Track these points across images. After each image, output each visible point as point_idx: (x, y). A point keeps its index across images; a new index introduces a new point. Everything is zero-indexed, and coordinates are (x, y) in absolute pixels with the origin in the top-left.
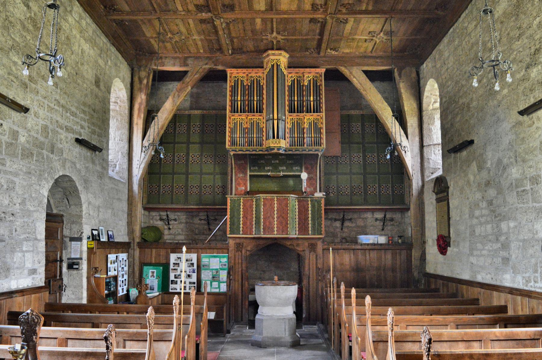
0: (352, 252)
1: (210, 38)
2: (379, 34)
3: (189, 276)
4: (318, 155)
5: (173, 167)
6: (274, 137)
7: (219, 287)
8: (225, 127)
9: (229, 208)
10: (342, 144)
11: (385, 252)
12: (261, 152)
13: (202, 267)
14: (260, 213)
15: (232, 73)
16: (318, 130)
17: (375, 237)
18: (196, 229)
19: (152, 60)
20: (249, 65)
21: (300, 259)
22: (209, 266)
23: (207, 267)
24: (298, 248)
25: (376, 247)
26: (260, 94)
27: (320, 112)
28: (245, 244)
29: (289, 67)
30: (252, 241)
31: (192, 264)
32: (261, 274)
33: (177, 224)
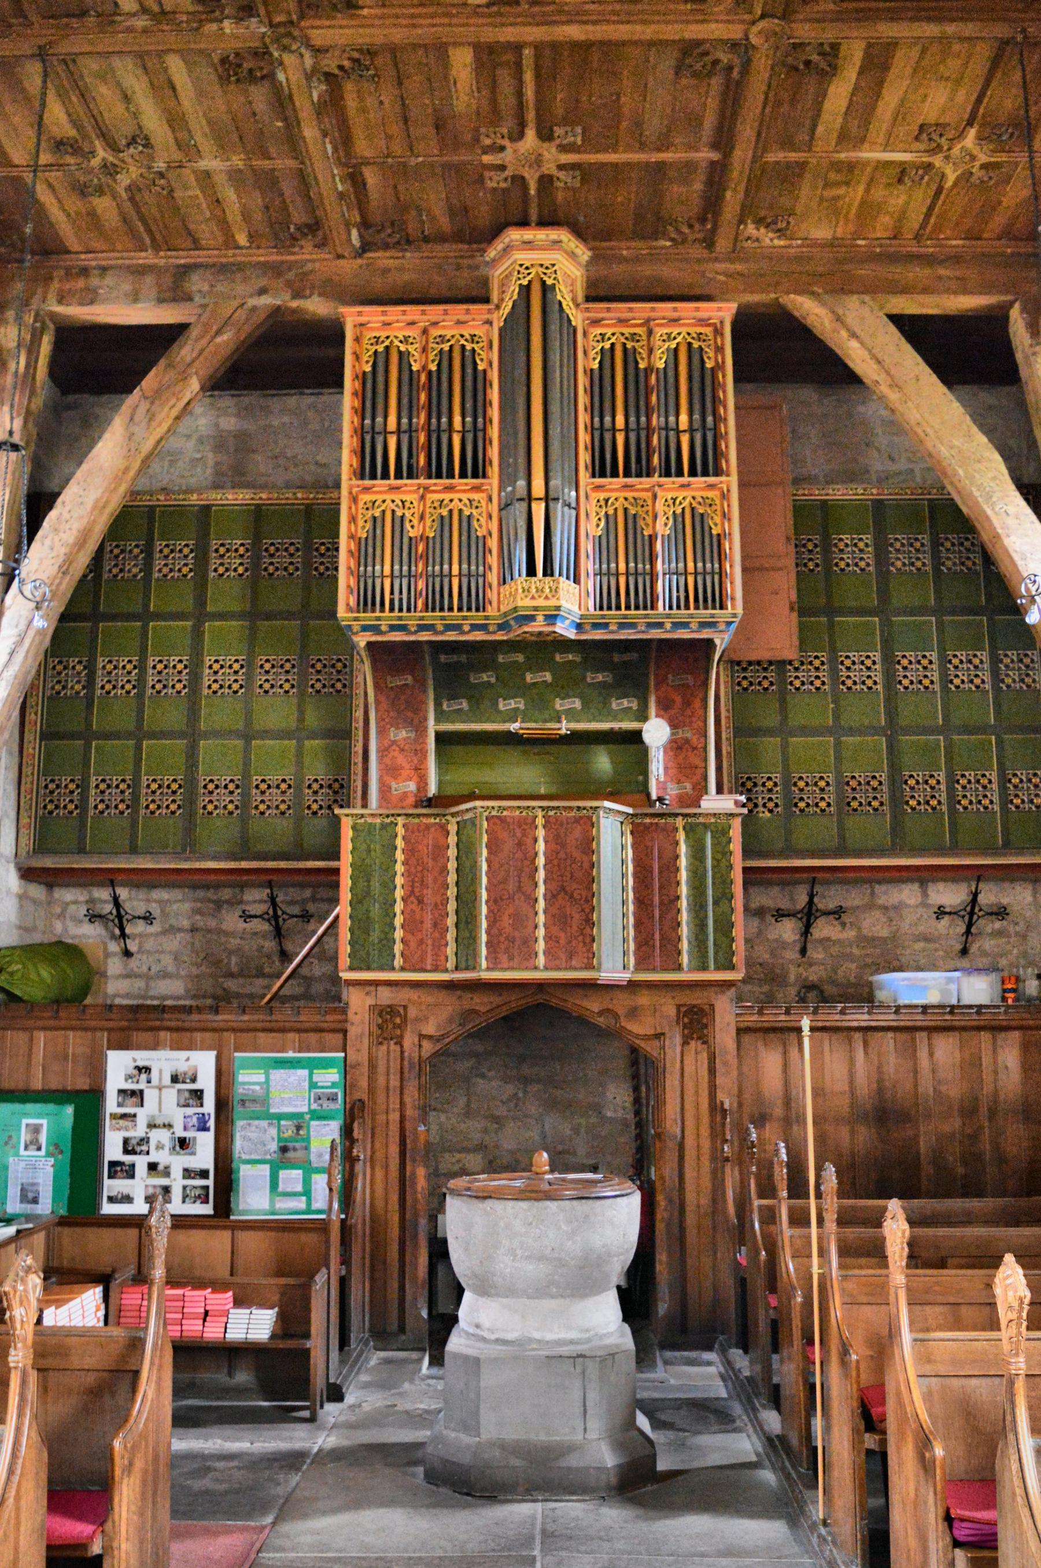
0: (858, 1036)
1: (266, 164)
2: (961, 135)
3: (183, 1144)
4: (709, 643)
5: (140, 711)
6: (531, 572)
7: (307, 1193)
8: (337, 535)
9: (346, 864)
10: (802, 612)
11: (994, 1038)
12: (478, 636)
13: (238, 1110)
14: (475, 880)
15: (371, 330)
16: (711, 547)
17: (949, 980)
18: (231, 953)
19: (48, 279)
20: (433, 292)
21: (642, 1071)
22: (263, 1101)
23: (260, 1106)
24: (635, 1027)
25: (957, 1020)
26: (477, 405)
27: (718, 472)
28: (412, 1012)
29: (593, 297)
30: (442, 996)
31: (198, 1095)
32: (485, 1131)
33: (157, 934)
